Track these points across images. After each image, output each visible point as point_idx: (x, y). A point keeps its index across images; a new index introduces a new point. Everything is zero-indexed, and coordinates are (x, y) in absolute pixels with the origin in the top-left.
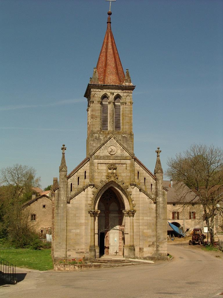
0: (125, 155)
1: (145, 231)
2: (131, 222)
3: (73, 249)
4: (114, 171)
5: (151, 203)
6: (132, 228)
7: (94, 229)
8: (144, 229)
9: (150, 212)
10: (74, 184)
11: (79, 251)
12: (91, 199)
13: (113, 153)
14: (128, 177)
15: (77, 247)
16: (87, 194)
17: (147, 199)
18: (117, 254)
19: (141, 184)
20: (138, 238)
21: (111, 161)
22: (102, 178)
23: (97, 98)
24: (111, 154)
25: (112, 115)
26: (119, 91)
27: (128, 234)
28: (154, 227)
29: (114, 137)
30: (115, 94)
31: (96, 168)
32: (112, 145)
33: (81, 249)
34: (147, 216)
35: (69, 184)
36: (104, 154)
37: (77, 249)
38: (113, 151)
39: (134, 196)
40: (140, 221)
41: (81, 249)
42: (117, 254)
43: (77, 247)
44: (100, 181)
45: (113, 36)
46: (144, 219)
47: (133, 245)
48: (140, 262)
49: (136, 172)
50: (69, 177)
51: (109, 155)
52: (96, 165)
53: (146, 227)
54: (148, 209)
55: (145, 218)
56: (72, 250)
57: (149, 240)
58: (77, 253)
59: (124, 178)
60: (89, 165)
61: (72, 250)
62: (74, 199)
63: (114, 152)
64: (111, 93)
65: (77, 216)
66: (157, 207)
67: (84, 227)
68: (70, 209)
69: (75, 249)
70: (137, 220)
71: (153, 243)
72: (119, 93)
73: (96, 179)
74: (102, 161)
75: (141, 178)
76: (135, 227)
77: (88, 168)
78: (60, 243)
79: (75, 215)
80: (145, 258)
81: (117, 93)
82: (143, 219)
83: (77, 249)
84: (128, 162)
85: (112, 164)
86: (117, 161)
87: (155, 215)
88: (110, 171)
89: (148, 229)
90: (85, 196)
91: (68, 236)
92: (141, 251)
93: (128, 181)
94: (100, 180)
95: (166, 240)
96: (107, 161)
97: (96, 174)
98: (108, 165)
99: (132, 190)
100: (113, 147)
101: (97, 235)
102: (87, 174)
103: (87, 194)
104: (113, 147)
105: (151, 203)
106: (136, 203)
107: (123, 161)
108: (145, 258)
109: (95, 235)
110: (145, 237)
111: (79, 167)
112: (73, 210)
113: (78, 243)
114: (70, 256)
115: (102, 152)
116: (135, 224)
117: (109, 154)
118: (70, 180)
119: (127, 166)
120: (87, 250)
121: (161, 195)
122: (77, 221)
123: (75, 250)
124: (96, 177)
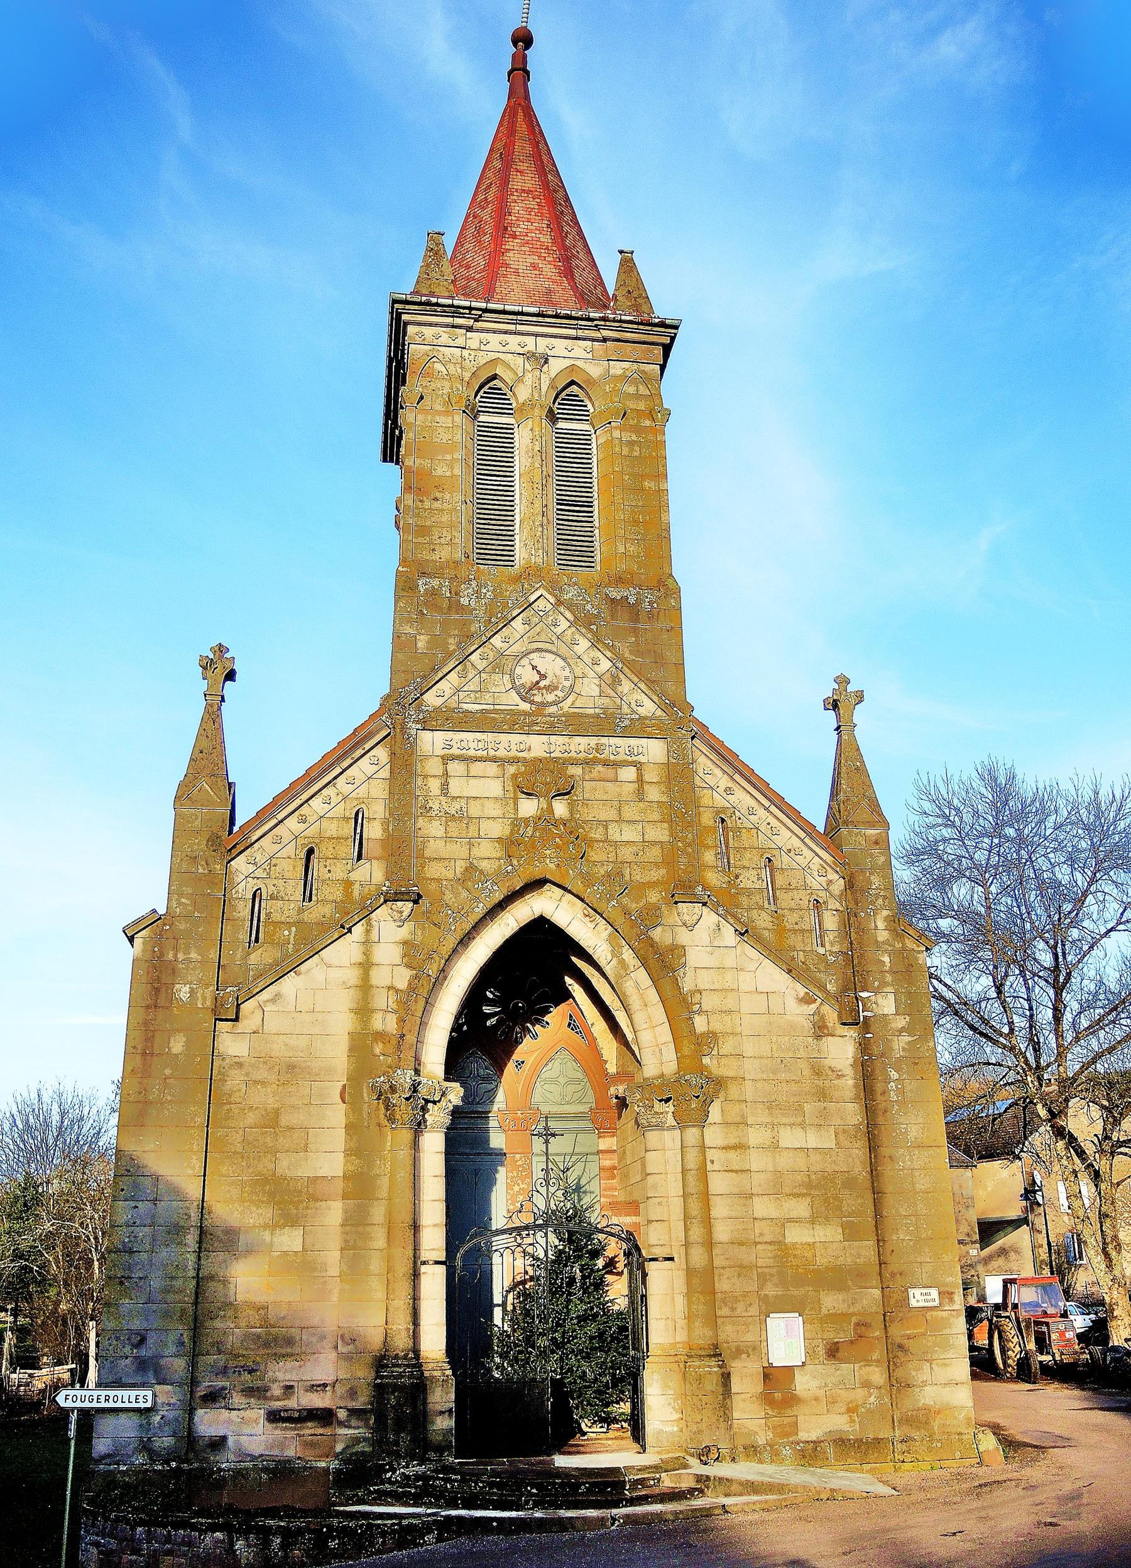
0: (626, 709)
1: (795, 1235)
2: (692, 1189)
3: (250, 1392)
4: (560, 808)
5: (820, 1030)
6: (695, 1208)
7: (416, 1227)
8: (790, 1220)
9: (822, 1095)
10: (272, 897)
11: (292, 1403)
12: (393, 997)
13: (550, 698)
14: (655, 853)
15: (280, 1375)
16: (366, 965)
17: (792, 1006)
18: (546, 1128)
19: (744, 900)
20: (746, 1294)
21: (537, 746)
22: (476, 852)
23: (447, 384)
24: (538, 699)
25: (537, 479)
26: (580, 349)
27: (671, 1259)
28: (859, 1203)
29: (552, 600)
30: (556, 366)
31: (435, 785)
32: (540, 645)
33: (314, 1388)
34: (802, 1125)
35: (244, 889)
36: (488, 698)
37: (276, 1390)
38: (542, 684)
39: (704, 980)
40: (757, 1161)
41: (314, 1388)
42: (546, 1128)
43: (281, 1372)
44: (459, 875)
45: (537, 122)
46: (782, 1144)
47: (716, 1346)
48: (779, 1488)
49: (707, 819)
50: (233, 851)
51: (525, 706)
52: (434, 767)
53: (801, 1208)
54: (807, 1072)
55: (790, 1138)
56: (237, 1399)
57: (831, 1301)
58: (274, 1417)
59: (626, 853)
60: (385, 773)
61: (237, 1399)
62: (273, 1001)
63: (551, 688)
64: (530, 356)
65: (289, 1128)
66: (864, 1046)
67: (334, 1213)
68: (234, 1072)
69: (266, 1389)
70: (732, 1155)
71: (857, 1324)
72: (579, 363)
73: (431, 859)
74: (470, 741)
75: (746, 863)
76: (720, 1209)
77: (379, 790)
78: (143, 1340)
79: (272, 1120)
80: (810, 1454)
81: (568, 363)
82: (775, 1146)
83: (276, 1390)
84: (654, 750)
85: (537, 765)
86: (581, 745)
87: (853, 1114)
88: (528, 807)
89: (813, 1221)
90: (352, 976)
91: (212, 1277)
92: (778, 1396)
93: (656, 874)
94: (460, 866)
95: (951, 1300)
96: (509, 743)
97: (435, 829)
98: (511, 770)
99: (684, 937)
100: (550, 664)
101: (442, 1269)
102: (373, 831)
103: (366, 965)
104: (550, 664)
105: (820, 1030)
106: (716, 1026)
107: (616, 746)
108: (810, 1454)
109: (423, 1269)
110: (799, 1282)
111: (310, 777)
112: (263, 1083)
113: (289, 1341)
114: (219, 1443)
115: (472, 686)
116: (718, 1183)
117: (524, 699)
118: (251, 868)
119: (647, 778)
120: (352, 1393)
121: (889, 978)
122: (285, 1165)
123: (257, 1392)
124: (434, 848)
